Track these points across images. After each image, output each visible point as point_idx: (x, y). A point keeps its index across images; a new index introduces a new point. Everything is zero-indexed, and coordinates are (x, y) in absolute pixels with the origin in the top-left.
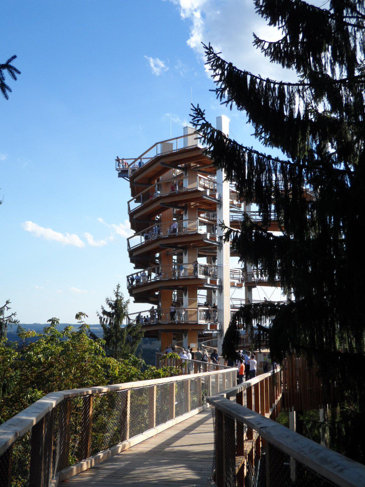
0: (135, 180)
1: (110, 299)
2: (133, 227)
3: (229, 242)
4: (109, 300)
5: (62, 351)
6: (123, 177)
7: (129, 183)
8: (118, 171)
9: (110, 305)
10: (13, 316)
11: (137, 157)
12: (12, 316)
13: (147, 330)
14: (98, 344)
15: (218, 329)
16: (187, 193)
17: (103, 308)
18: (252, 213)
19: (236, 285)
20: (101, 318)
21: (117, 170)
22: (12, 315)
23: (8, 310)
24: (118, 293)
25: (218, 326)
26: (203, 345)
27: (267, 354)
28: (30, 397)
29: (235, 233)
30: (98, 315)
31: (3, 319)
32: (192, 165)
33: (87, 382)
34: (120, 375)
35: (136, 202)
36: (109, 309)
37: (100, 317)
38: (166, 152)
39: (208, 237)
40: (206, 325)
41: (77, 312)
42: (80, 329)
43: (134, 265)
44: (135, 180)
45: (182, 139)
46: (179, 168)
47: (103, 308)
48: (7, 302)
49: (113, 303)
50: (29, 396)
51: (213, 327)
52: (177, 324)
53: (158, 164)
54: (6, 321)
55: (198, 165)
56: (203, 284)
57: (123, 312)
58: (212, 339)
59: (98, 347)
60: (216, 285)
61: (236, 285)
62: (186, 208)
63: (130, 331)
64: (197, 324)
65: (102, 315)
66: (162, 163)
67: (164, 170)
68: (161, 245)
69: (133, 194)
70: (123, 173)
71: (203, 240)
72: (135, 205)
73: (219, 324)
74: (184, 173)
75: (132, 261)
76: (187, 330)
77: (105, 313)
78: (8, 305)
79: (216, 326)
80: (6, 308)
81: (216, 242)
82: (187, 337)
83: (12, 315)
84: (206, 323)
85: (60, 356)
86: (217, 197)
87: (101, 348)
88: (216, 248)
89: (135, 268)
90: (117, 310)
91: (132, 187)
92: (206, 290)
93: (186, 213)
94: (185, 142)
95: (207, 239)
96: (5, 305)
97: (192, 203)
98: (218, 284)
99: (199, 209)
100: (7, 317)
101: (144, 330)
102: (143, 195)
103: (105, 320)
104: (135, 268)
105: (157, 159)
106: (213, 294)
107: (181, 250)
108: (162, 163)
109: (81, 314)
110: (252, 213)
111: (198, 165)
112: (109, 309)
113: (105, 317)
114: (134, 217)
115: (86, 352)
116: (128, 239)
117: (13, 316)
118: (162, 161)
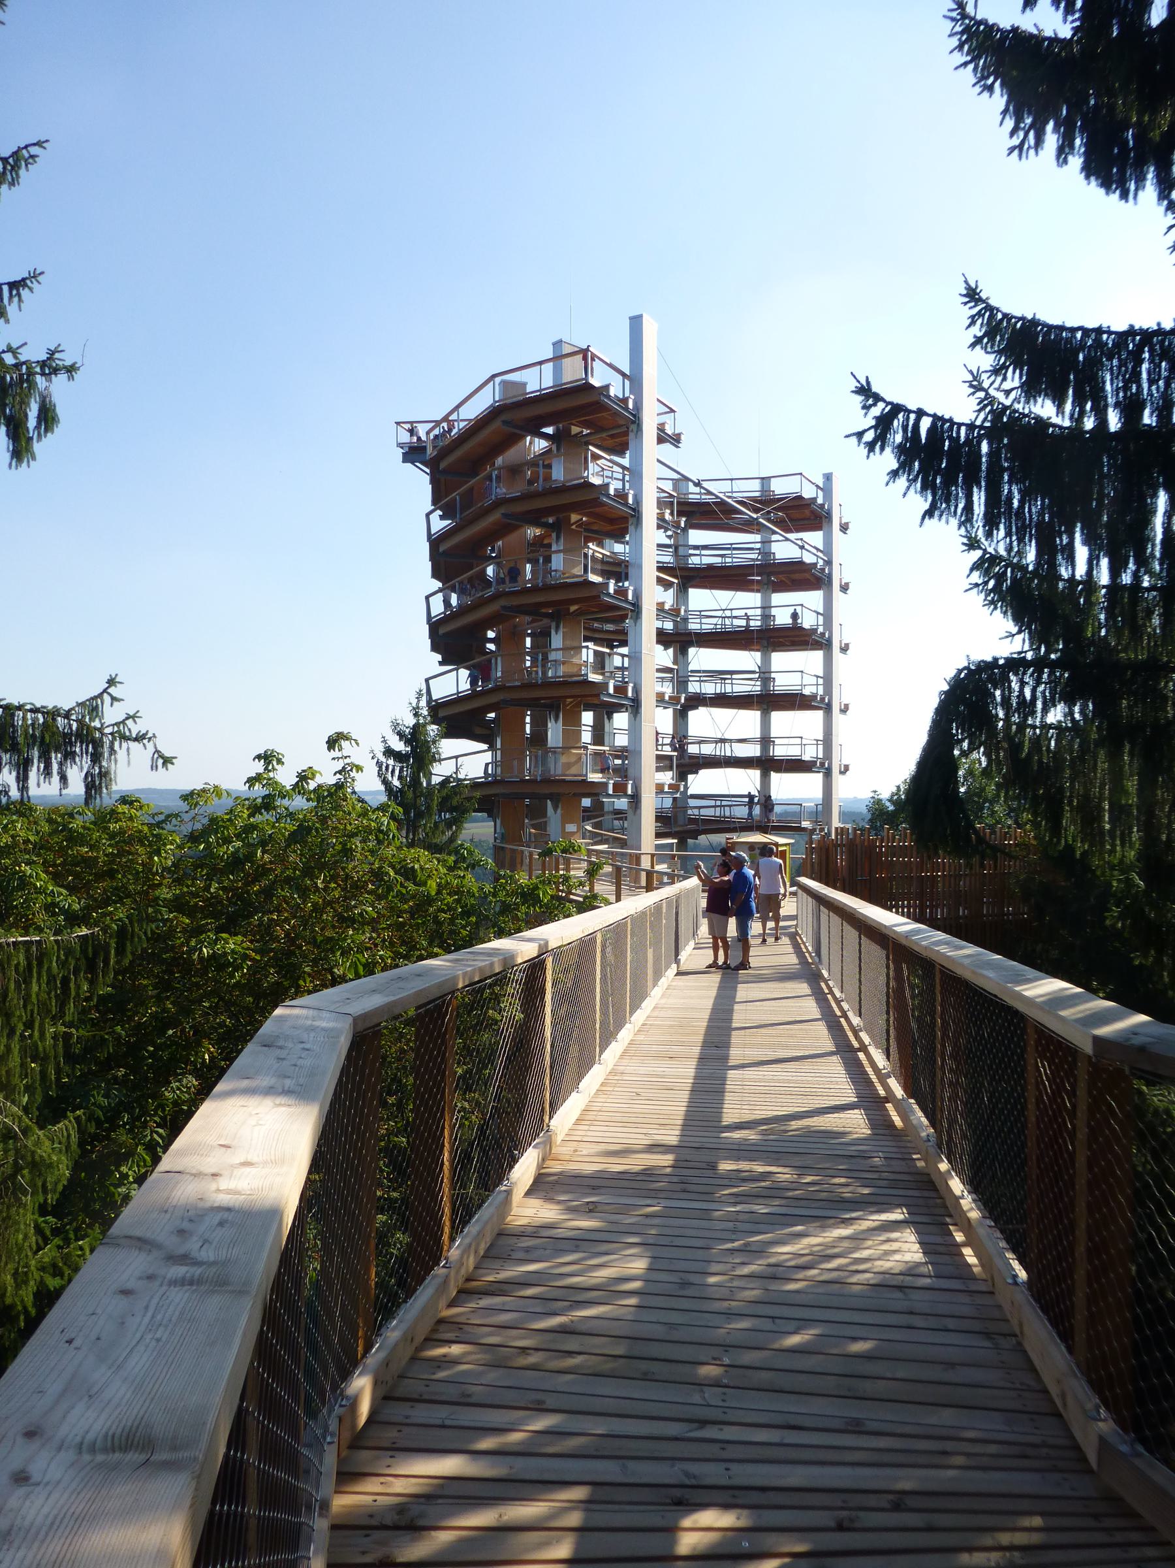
0: (442, 465)
1: (400, 721)
2: (436, 574)
3: (888, 450)
4: (398, 724)
5: (293, 834)
6: (413, 463)
7: (428, 478)
8: (402, 448)
9: (401, 735)
10: (129, 722)
11: (439, 418)
12: (127, 722)
13: (484, 793)
14: (384, 815)
15: (629, 792)
16: (564, 489)
17: (385, 741)
18: (691, 552)
19: (667, 698)
20: (380, 765)
21: (400, 445)
22: (127, 719)
23: (115, 703)
24: (418, 708)
25: (630, 787)
26: (589, 828)
27: (757, 846)
28: (208, 952)
29: (913, 416)
30: (373, 758)
31: (100, 730)
32: (575, 430)
33: (362, 913)
34: (439, 892)
35: (442, 518)
36: (399, 746)
37: (377, 762)
38: (515, 397)
39: (611, 591)
40: (605, 785)
41: (331, 732)
42: (338, 776)
43: (439, 657)
44: (442, 465)
45: (551, 364)
46: (546, 436)
47: (385, 741)
48: (112, 682)
49: (407, 731)
50: (205, 950)
51: (620, 789)
52: (541, 781)
53: (496, 425)
54: (110, 736)
55: (585, 432)
56: (598, 695)
57: (430, 752)
58: (603, 815)
59: (386, 823)
60: (626, 697)
61: (667, 698)
62: (559, 527)
63: (447, 794)
64: (584, 781)
65: (383, 759)
66: (504, 422)
67: (513, 439)
68: (504, 608)
69: (436, 501)
70: (413, 453)
71: (599, 597)
72: (439, 524)
73: (631, 782)
74: (554, 448)
75: (435, 648)
76: (558, 794)
77: (389, 752)
78: (111, 690)
79: (626, 786)
80: (106, 697)
81: (626, 601)
82: (559, 811)
83: (127, 719)
84: (604, 780)
85: (288, 846)
86: (630, 501)
87: (393, 825)
88: (625, 617)
89: (441, 663)
90: (417, 747)
91: (434, 482)
92: (591, 713)
93: (558, 538)
94: (557, 372)
95: (609, 594)
96: (105, 691)
97: (574, 517)
98: (630, 694)
99: (587, 530)
100: (113, 725)
101: (478, 794)
102: (462, 496)
103: (390, 770)
104: (441, 663)
105: (494, 413)
106: (606, 721)
107: (545, 621)
108: (504, 422)
109: (346, 737)
110: (691, 552)
111: (585, 432)
112: (399, 746)
113: (391, 762)
114: (441, 550)
115: (355, 835)
116: (427, 598)
117: (129, 722)
118: (504, 417)
